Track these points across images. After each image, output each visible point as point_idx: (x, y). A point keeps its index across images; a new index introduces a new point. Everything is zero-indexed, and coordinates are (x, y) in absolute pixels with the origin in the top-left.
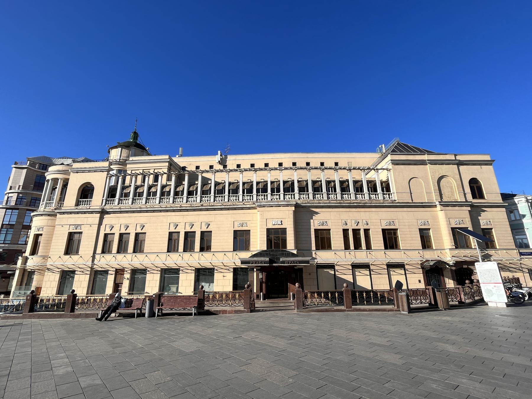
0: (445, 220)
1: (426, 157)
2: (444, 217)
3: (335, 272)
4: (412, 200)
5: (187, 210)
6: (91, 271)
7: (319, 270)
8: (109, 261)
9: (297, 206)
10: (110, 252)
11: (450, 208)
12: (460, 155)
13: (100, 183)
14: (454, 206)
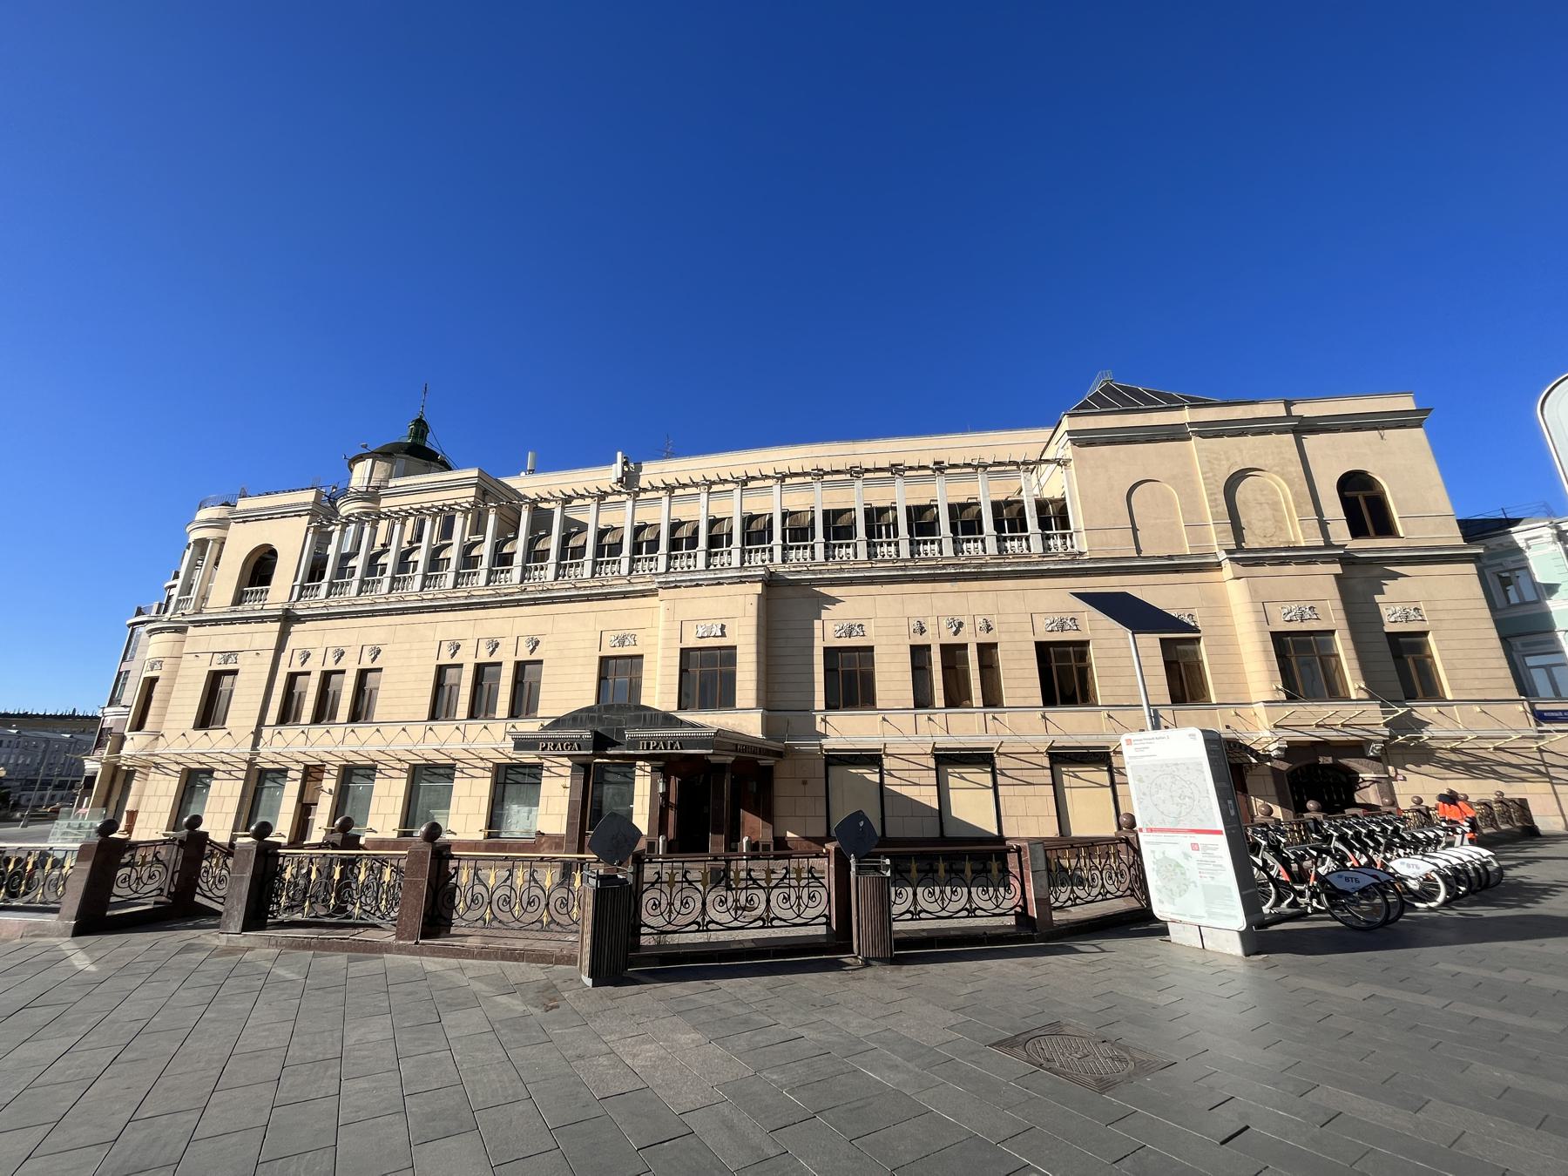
0: (1249, 607)
1: (1185, 416)
2: (1248, 599)
3: (882, 778)
4: (1139, 551)
5: (484, 606)
6: (248, 772)
7: (834, 771)
8: (292, 745)
9: (772, 582)
10: (449, 715)
11: (1267, 569)
12: (1304, 401)
13: (291, 541)
14: (1283, 561)
